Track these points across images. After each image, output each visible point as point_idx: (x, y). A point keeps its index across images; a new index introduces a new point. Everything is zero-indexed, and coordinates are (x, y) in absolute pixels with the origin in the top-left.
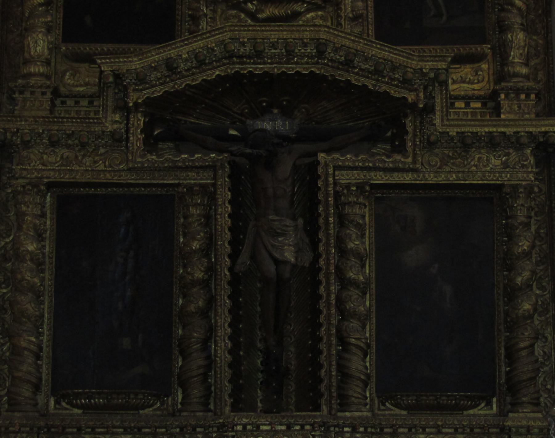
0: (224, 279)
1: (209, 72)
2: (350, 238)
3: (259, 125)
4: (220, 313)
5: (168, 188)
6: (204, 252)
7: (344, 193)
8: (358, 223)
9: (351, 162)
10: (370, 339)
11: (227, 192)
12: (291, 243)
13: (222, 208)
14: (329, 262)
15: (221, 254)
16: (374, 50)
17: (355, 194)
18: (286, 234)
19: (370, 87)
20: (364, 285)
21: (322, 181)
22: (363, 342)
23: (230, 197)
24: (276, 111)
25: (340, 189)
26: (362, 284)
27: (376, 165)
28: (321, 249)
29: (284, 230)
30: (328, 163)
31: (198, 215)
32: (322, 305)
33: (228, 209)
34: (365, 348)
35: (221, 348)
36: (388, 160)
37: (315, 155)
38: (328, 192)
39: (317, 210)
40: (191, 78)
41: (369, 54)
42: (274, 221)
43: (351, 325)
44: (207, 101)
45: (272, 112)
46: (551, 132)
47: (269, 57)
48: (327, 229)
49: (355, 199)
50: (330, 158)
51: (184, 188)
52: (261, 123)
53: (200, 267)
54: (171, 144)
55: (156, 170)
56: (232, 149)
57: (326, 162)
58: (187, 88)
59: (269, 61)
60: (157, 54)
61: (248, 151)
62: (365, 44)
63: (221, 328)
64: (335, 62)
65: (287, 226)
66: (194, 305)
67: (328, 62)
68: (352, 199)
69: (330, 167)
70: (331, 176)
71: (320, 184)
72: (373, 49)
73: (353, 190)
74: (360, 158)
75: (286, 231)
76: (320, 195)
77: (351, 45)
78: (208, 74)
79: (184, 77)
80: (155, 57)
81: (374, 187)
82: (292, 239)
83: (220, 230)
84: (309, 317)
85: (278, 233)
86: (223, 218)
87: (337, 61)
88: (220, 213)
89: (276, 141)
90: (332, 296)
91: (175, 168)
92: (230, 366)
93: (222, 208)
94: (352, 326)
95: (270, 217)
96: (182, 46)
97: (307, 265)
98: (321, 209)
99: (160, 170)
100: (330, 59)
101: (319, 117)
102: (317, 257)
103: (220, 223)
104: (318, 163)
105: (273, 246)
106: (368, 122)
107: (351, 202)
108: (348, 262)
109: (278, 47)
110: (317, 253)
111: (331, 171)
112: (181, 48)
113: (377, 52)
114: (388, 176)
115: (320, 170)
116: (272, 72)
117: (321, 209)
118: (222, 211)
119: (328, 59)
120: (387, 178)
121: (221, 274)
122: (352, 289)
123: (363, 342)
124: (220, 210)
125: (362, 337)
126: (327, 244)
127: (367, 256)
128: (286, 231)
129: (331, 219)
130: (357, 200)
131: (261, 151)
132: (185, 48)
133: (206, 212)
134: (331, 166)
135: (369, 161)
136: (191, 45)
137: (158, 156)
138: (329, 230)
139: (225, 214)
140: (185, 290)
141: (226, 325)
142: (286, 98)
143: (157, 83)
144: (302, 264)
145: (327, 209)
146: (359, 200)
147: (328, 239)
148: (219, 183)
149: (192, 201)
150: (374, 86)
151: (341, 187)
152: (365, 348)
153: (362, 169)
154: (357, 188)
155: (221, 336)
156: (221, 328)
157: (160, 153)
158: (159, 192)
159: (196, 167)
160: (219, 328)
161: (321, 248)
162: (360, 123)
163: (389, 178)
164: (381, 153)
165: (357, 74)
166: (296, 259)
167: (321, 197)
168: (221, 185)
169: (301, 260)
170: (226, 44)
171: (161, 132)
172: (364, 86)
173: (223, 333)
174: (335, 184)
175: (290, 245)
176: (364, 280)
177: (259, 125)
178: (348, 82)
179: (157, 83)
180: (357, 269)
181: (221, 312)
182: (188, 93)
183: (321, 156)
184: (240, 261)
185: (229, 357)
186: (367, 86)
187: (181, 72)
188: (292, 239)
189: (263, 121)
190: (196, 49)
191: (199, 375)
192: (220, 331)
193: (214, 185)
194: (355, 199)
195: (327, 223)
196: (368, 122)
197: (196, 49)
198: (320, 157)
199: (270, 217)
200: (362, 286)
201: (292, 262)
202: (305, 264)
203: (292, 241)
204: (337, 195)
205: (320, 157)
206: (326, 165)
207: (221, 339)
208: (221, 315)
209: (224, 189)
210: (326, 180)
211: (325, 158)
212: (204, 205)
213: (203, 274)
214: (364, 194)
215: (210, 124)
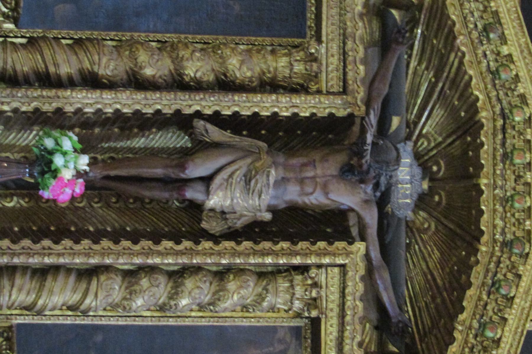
0: (185, 103)
1: (482, 86)
2: (241, 287)
3: (407, 160)
4: (134, 97)
5: (315, 28)
6: (223, 77)
7: (306, 280)
8: (263, 299)
9: (353, 290)
10: (94, 316)
11: (309, 110)
12: (235, 201)
13: (287, 102)
14: (208, 255)
15: (221, 101)
16: (514, 321)
17: (306, 295)
18: (249, 194)
19: (461, 317)
20: (174, 307)
21: (325, 249)
22: (91, 304)
23: (302, 114)
24: (425, 186)
25: (313, 273)
26: (175, 305)
27: (348, 325)
28: (227, 245)
29: (253, 191)
30: (351, 255)
31: (276, 69)
32: (146, 243)
33: (284, 112)
34: (82, 307)
35: (84, 98)
36: (354, 344)
37: (363, 238)
38: (309, 255)
39: (284, 240)
40: (474, 59)
41: (509, 314)
42: (268, 176)
43: (117, 287)
44: (440, 85)
45: (423, 178)
46: (502, 28)
47: (504, 172)
48: (255, 253)
49: (298, 296)
50: (358, 259)
51: (316, 49)
52: (408, 164)
53: (202, 70)
54: (377, 34)
55: (341, 9)
56: (372, 116)
57: (352, 253)
58: (460, 54)
59: (498, 172)
60: (508, 10)
61: (369, 139)
62: (523, 309)
63: (113, 98)
64: (498, 266)
65: (260, 196)
66: (147, 61)
67: (497, 256)
68: (299, 291)
69: (344, 259)
70: (332, 261)
71: (322, 244)
72: (517, 320)
73: (311, 292)
74: (358, 303)
75: (252, 194)
76: (305, 244)
77: (521, 290)
78: (479, 85)
79: (475, 49)
80: (504, 6)
81: (315, 323)
82: (241, 202)
83: (255, 100)
84: (128, 229)
85: (250, 181)
86: (272, 104)
87: (499, 269)
88: (279, 100)
89: (383, 180)
90: (158, 259)
91: (344, 38)
92: (59, 111)
93: (287, 102)
94: (115, 288)
95: (273, 172)
96: (520, 46)
97: (204, 225)
98: (284, 245)
99: (340, 15)
100: (502, 259)
101: (417, 247)
102: (216, 239)
103: (264, 99)
104: (351, 243)
105: (231, 176)
106: (435, 60)
107: (293, 289)
108: (208, 284)
109: (518, 185)
110: (220, 239)
111: (340, 261)
112: (516, 44)
113: (512, 327)
114: (331, 344)
115: (340, 245)
116: (482, 175)
117: (284, 245)
118: (282, 102)
119: (501, 256)
120: (329, 342)
121: (192, 100)
122: (169, 289)
123: (91, 304)
124: (284, 100)
125: (98, 302)
126: (235, 254)
127: (216, 312)
128: (252, 194)
129: (269, 260)
130: (298, 299)
131: (368, 157)
132: (517, 51)
133: (280, 81)
134: (347, 261)
135: (354, 316)
136: (521, 58)
137: (361, 15)
138: (254, 257)
139: (278, 107)
140: (168, 49)
141: (118, 106)
142: (444, 202)
143: (467, 11)
144: (205, 218)
145: (283, 253)
146: (297, 302)
147: (240, 254)
148: (322, 100)
149: (296, 60)
150: (463, 323)
151: (317, 274)
152: (82, 307)
153: (342, 306)
154: (315, 299)
155: (103, 98)
156: (113, 98)
157: (365, 19)
158: (309, 15)
159: (345, 67)
160: (113, 96)
161: (228, 244)
162: (407, 307)
163: (329, 344)
164: (364, 337)
165: (480, 299)
166: (212, 210)
167: (303, 245)
168: (320, 102)
169: (211, 217)
170: (523, 109)
171: (395, 19)
172: (462, 309)
173: (107, 102)
174: (319, 266)
175: (232, 200)
176: (181, 306)
177: (407, 160)
178: (469, 285)
179: (467, 11)
180: (197, 296)
181: (137, 99)
182: (452, 56)
183: (360, 247)
184: (209, 126)
185: (69, 109)
186: (462, 312)
187: (482, 45)
188: (241, 202)
189: (411, 166)
190: (515, 66)
191: (46, 67)
192: (109, 97)
193: (319, 92)
194: (298, 296)
195: (264, 253)
196: (435, 60)
197: (515, 66)
198: (359, 246)
199: (273, 172)
200: (172, 303)
201: (207, 202)
202: (204, 222)
203: (238, 203)
204: (303, 269)
205: (359, 246)
206: (348, 254)
207: (97, 98)
208: (133, 99)
209: (314, 107)
210: (326, 254)
211: (357, 252)
212: (290, 77)
213: (192, 75)
214: (306, 309)
215: (406, 90)
